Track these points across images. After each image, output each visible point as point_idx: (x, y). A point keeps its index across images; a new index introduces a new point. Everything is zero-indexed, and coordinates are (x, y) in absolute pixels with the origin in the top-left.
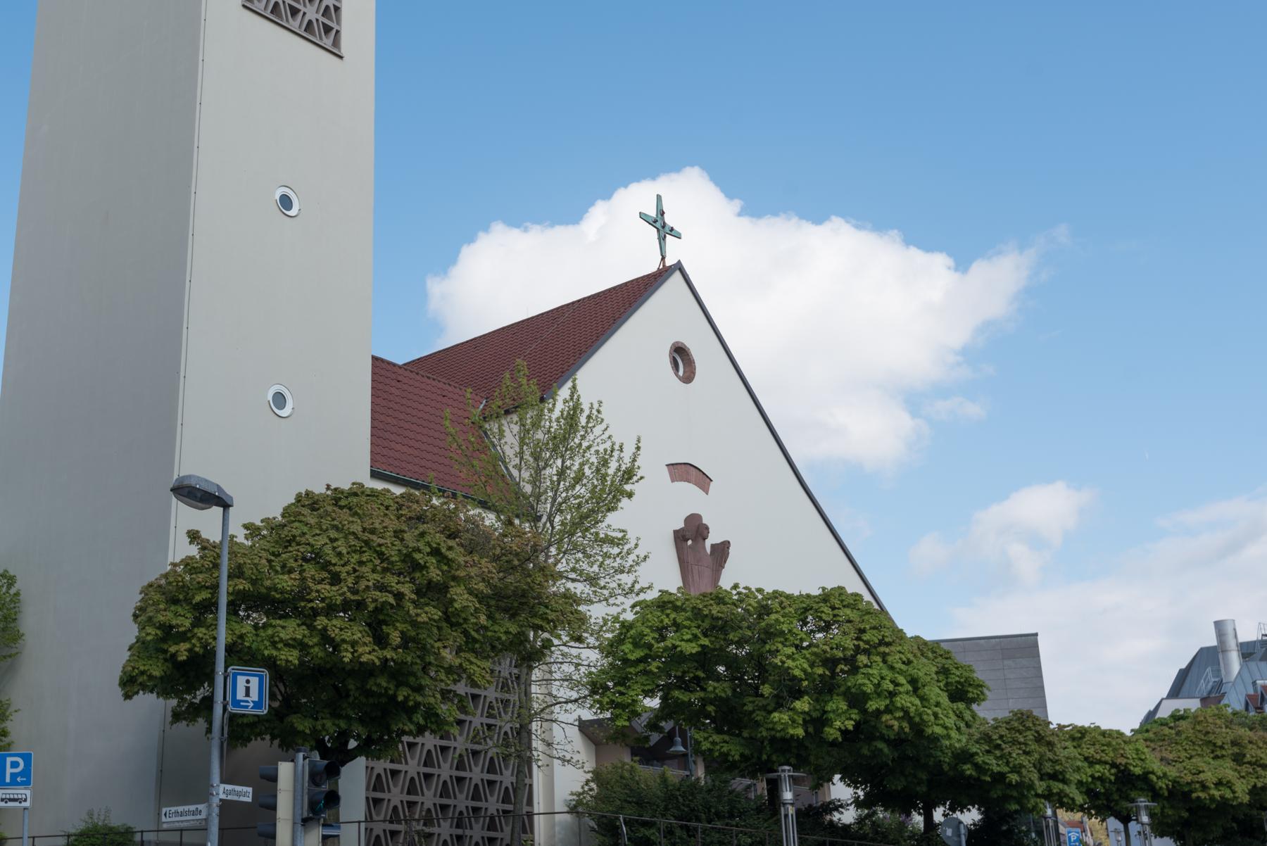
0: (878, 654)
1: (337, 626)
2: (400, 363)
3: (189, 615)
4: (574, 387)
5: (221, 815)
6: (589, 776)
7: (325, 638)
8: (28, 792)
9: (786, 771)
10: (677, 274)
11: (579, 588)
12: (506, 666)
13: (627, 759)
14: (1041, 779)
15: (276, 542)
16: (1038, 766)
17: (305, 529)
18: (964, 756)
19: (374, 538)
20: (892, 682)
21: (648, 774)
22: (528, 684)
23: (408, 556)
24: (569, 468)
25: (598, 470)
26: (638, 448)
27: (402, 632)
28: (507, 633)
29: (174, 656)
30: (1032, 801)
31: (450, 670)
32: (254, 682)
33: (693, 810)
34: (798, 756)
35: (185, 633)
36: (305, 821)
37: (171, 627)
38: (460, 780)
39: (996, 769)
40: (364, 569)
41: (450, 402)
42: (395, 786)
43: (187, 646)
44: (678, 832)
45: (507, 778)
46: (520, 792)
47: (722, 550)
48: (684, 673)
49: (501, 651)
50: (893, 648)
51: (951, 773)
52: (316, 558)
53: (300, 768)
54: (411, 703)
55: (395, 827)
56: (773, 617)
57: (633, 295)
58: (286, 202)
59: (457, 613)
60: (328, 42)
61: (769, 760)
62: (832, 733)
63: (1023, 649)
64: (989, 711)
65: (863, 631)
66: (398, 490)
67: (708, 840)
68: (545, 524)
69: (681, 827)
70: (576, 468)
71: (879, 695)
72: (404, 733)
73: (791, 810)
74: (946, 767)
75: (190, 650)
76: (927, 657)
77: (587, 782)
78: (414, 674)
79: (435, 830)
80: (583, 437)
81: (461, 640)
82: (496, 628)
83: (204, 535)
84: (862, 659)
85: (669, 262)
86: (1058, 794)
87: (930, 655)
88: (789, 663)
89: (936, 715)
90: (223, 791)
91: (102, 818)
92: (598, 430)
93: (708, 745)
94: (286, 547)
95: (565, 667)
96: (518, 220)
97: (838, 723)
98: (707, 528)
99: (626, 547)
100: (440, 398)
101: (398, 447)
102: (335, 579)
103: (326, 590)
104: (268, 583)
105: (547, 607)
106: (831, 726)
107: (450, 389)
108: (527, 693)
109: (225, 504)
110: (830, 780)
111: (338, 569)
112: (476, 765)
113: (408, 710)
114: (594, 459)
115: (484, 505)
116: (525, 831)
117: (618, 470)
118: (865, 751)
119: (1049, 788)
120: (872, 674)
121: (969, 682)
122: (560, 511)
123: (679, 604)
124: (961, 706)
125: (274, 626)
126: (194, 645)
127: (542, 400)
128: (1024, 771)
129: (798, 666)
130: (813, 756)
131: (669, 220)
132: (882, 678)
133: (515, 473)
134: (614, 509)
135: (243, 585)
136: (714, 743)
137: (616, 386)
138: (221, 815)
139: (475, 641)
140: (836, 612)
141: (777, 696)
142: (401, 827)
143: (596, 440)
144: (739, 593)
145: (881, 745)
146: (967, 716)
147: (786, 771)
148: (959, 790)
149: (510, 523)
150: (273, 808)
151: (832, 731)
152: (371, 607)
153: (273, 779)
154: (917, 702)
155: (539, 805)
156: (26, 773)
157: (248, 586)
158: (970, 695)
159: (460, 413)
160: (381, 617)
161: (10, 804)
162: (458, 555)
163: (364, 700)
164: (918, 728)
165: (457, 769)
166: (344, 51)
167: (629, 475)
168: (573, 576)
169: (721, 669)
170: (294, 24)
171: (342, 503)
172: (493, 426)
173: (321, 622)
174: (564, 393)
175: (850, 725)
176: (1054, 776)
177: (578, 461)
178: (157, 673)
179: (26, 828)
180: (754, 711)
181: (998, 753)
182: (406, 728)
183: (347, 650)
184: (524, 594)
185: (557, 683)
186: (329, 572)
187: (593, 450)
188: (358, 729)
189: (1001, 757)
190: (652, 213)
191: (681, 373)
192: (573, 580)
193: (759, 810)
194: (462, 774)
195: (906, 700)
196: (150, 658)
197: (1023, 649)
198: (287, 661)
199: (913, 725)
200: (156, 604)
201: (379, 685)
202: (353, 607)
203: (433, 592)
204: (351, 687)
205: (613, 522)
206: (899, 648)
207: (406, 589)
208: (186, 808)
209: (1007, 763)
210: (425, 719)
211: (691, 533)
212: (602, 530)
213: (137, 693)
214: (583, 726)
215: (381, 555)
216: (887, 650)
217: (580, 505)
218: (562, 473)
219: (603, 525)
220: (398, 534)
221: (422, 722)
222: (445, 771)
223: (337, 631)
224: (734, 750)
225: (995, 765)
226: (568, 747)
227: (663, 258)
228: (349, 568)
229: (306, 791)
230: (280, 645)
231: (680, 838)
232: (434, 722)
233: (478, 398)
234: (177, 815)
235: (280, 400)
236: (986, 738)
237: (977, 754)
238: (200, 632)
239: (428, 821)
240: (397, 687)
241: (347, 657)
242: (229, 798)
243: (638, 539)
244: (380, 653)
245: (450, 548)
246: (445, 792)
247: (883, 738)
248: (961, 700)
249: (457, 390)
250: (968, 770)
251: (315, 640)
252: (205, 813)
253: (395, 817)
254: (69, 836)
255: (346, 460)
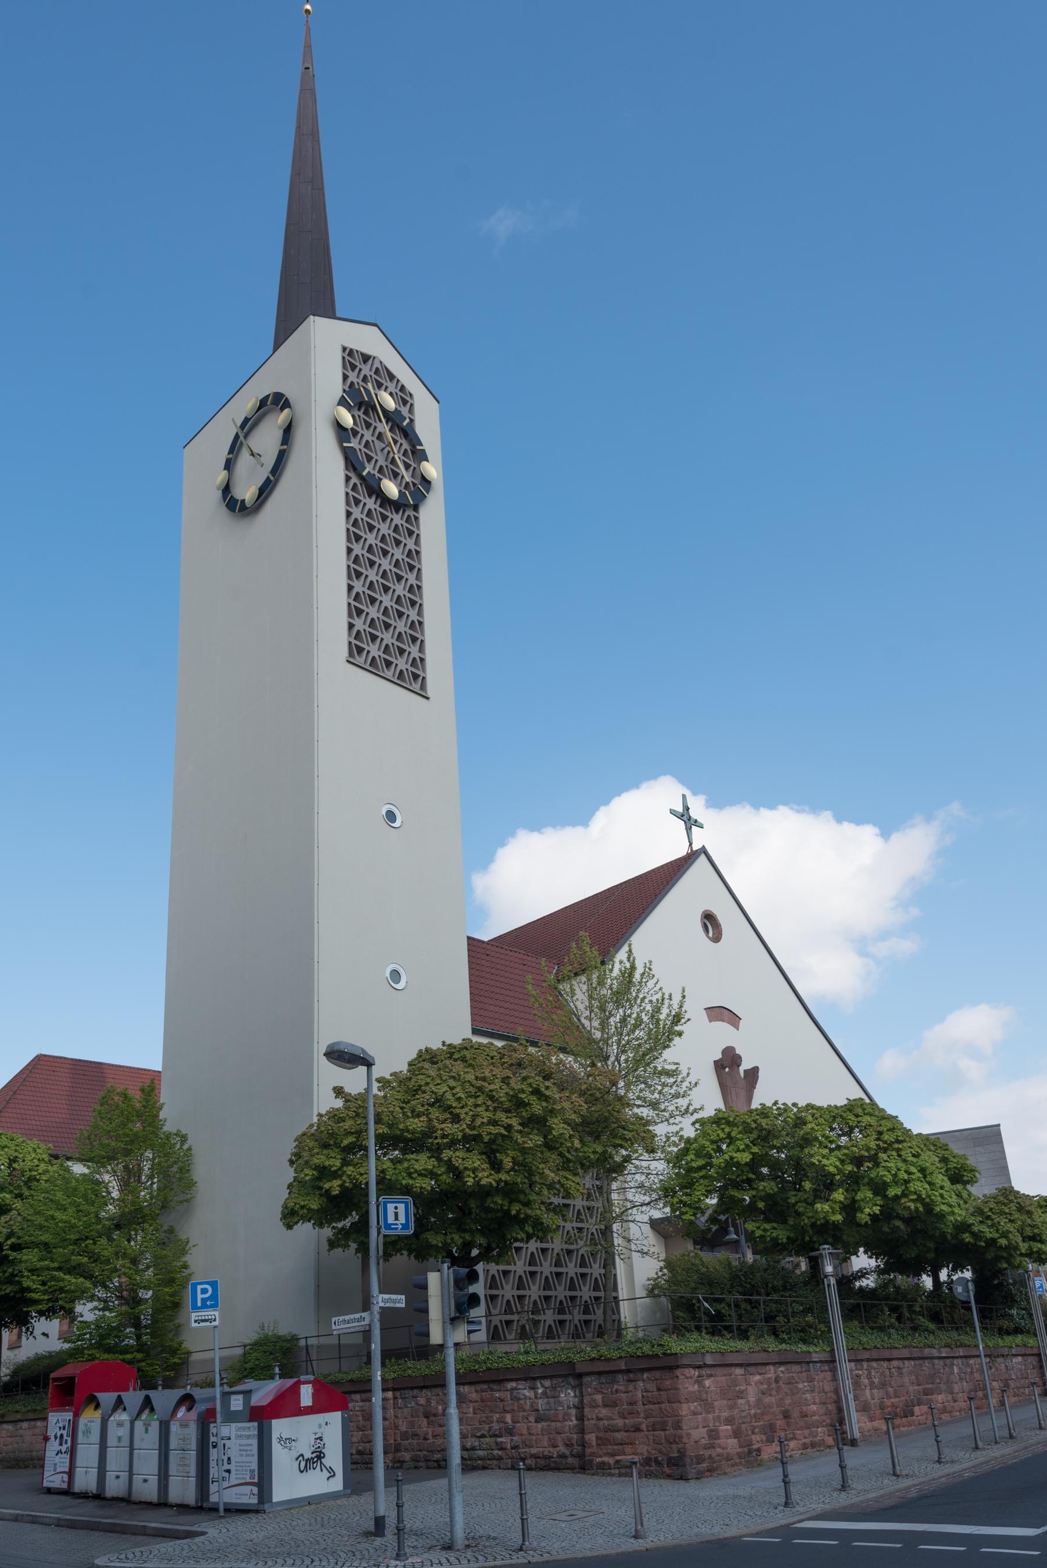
0: (894, 1149)
1: (457, 1156)
2: (486, 939)
3: (339, 1157)
4: (630, 951)
5: (381, 1321)
6: (662, 1264)
7: (451, 1167)
8: (217, 1313)
9: (826, 1249)
10: (703, 857)
11: (645, 1112)
12: (588, 1181)
13: (690, 1246)
14: (1024, 1241)
15: (406, 1092)
16: (1021, 1231)
17: (428, 1080)
18: (963, 1227)
19: (486, 1084)
20: (906, 1172)
21: (713, 1259)
22: (609, 1193)
23: (515, 1096)
24: (629, 1016)
25: (653, 1016)
26: (684, 997)
27: (513, 1158)
28: (595, 1152)
29: (328, 1191)
30: (1018, 1259)
31: (550, 1187)
32: (401, 1207)
33: (753, 1286)
34: (834, 1236)
35: (336, 1172)
36: (453, 1320)
37: (324, 1168)
38: (558, 1275)
39: (989, 1236)
40: (479, 1109)
41: (530, 969)
42: (507, 1283)
43: (339, 1182)
44: (743, 1306)
45: (596, 1270)
46: (607, 1283)
47: (753, 1074)
48: (737, 1178)
49: (589, 1168)
50: (905, 1144)
51: (953, 1242)
52: (439, 1102)
53: (446, 1276)
54: (522, 1216)
55: (509, 1317)
56: (809, 1126)
57: (667, 876)
58: (391, 816)
59: (555, 1139)
60: (416, 687)
61: (811, 1241)
62: (863, 1217)
63: (990, 1137)
64: (982, 1189)
65: (880, 1133)
66: (499, 1044)
67: (768, 1310)
68: (613, 1064)
69: (745, 1300)
70: (634, 1016)
71: (896, 1183)
72: (516, 1240)
73: (833, 1281)
74: (949, 1237)
75: (341, 1186)
76: (930, 1150)
77: (661, 1269)
78: (523, 1192)
79: (542, 1317)
80: (639, 991)
81: (559, 1160)
82: (586, 1149)
83: (347, 1090)
84: (883, 1156)
85: (696, 847)
86: (1038, 1252)
87: (932, 1148)
88: (825, 1162)
89: (942, 1196)
90: (381, 1300)
91: (272, 1328)
92: (651, 984)
93: (761, 1232)
94: (414, 1095)
95: (637, 1177)
96: (536, 826)
97: (867, 1210)
98: (740, 1057)
99: (680, 1077)
100: (521, 967)
101: (492, 1008)
102: (456, 1119)
103: (450, 1128)
104: (401, 1126)
105: (624, 1129)
106: (862, 1212)
107: (529, 958)
108: (609, 1200)
109: (368, 1063)
110: (856, 1253)
111: (458, 1111)
112: (570, 1261)
113: (519, 1221)
114: (649, 1008)
115: (563, 1050)
116: (614, 1313)
117: (668, 1015)
118: (886, 1229)
119: (1030, 1248)
120: (890, 1165)
121: (964, 1168)
122: (624, 1052)
123: (731, 1119)
124: (959, 1187)
125: (409, 1160)
126: (345, 1181)
127: (603, 963)
128: (1011, 1236)
129: (831, 1164)
130: (843, 1237)
131: (694, 814)
132: (899, 1170)
133: (586, 1023)
134: (668, 1046)
135: (383, 1129)
136: (765, 1230)
137: (659, 946)
138: (382, 1321)
139: (569, 1161)
140: (859, 1119)
141: (815, 1190)
142: (515, 1317)
143: (649, 992)
144: (779, 1108)
145: (898, 1223)
146: (965, 1195)
147: (826, 1249)
148: (956, 1251)
149: (593, 1065)
150: (426, 1311)
151: (863, 1216)
152: (486, 1139)
153: (425, 1287)
154: (927, 1186)
155: (623, 1293)
156: (214, 1297)
157: (386, 1130)
158: (965, 1178)
159: (538, 977)
160: (494, 1147)
161: (202, 1324)
162: (554, 1093)
163: (484, 1216)
164: (929, 1208)
165: (556, 1266)
166: (429, 694)
167: (677, 1019)
168: (639, 1102)
169: (765, 1170)
170: (389, 674)
171: (456, 1056)
172: (564, 987)
173: (446, 1154)
174: (622, 955)
175: (877, 1210)
176: (1034, 1238)
177: (636, 1009)
178: (315, 1206)
179: (217, 1343)
180: (797, 1203)
181: (989, 1222)
182: (519, 1237)
183: (469, 1176)
184: (606, 1119)
185: (633, 1190)
186: (451, 1113)
187: (646, 1001)
188: (481, 1240)
189: (992, 1226)
190: (680, 809)
191: (711, 935)
192: (639, 1106)
193: (806, 1283)
194: (560, 1270)
195: (918, 1186)
196: (308, 1194)
197: (990, 1137)
198: (421, 1188)
199: (926, 1205)
200: (311, 1149)
201: (495, 1203)
202: (470, 1141)
203: (537, 1123)
204: (473, 1205)
205: (669, 1056)
206: (909, 1144)
207: (514, 1122)
208: (352, 1316)
209: (997, 1231)
210: (533, 1228)
211: (727, 1064)
212: (659, 1065)
213: (296, 1223)
214: (654, 1224)
215: (492, 1098)
216: (900, 1146)
217: (640, 1045)
218: (624, 1020)
219: (661, 1059)
220: (505, 1080)
221: (530, 1230)
222: (546, 1268)
223: (460, 1161)
224: (782, 1234)
225: (989, 1233)
226: (645, 1242)
227: (691, 844)
228: (466, 1110)
229: (452, 1295)
230: (415, 1175)
231: (745, 1310)
232: (541, 1231)
233: (551, 965)
234: (346, 1324)
235: (396, 975)
236: (979, 1211)
237: (973, 1224)
238: (349, 1170)
239: (535, 1311)
240: (510, 1203)
241: (470, 1181)
242: (387, 1305)
243: (689, 1069)
244: (496, 1176)
245: (547, 1088)
246: (547, 1286)
247: (899, 1217)
248: (958, 1182)
249: (534, 960)
250: (967, 1238)
251: (443, 1169)
252: (371, 1319)
253: (508, 1309)
254: (245, 1346)
255: (451, 1022)
